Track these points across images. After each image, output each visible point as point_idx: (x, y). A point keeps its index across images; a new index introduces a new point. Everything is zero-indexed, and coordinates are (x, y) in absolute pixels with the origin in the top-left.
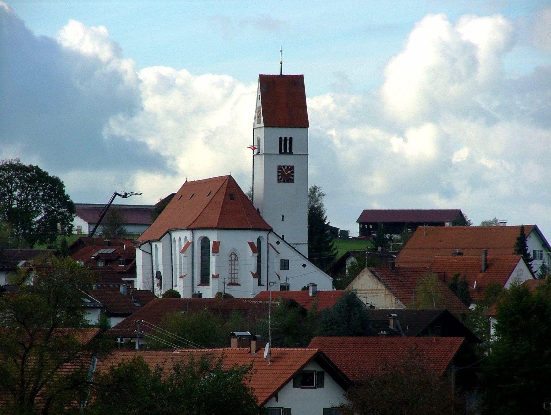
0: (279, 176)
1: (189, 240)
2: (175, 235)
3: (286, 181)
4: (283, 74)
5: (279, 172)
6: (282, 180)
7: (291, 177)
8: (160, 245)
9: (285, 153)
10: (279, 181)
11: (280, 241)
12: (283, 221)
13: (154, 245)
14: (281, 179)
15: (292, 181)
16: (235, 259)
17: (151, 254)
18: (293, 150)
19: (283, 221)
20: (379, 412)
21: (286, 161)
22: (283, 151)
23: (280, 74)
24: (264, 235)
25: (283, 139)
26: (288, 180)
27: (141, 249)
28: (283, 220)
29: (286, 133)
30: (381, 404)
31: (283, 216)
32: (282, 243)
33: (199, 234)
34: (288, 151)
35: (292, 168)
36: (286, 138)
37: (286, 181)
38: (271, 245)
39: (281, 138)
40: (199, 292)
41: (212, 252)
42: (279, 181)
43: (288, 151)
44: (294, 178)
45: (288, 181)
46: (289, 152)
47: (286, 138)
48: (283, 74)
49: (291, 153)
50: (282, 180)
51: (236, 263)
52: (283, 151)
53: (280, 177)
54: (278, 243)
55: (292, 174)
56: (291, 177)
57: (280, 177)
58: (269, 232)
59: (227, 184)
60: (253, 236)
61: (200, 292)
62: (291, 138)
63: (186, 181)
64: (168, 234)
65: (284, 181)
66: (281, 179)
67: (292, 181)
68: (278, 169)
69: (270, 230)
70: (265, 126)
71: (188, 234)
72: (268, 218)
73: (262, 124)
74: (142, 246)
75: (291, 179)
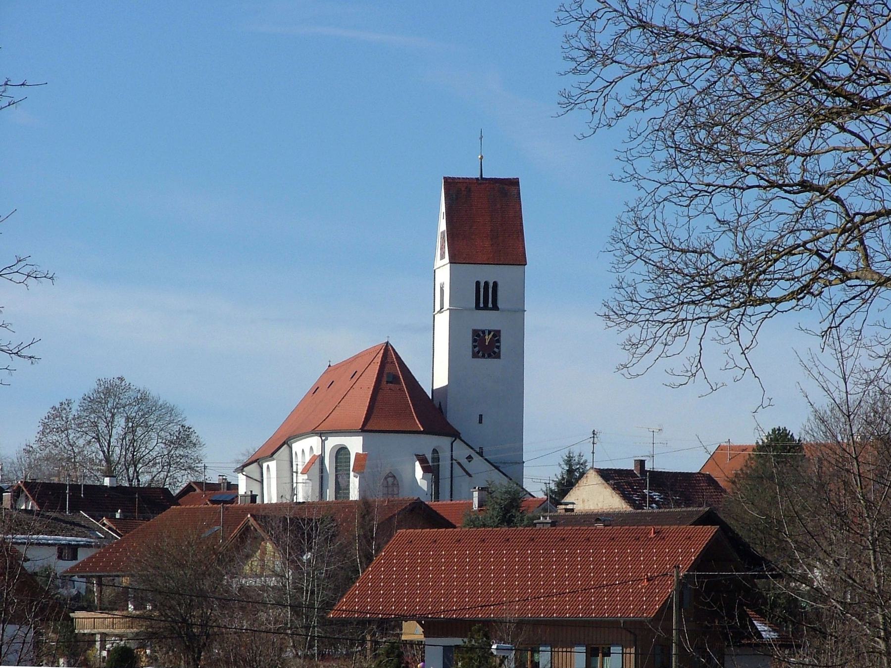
0: (475, 347)
1: (317, 452)
2: (297, 446)
3: (486, 356)
4: (483, 177)
5: (474, 341)
6: (480, 354)
7: (496, 350)
8: (273, 464)
9: (486, 308)
10: (475, 355)
11: (473, 454)
12: (481, 423)
13: (265, 465)
14: (478, 352)
15: (497, 356)
16: (393, 484)
17: (262, 482)
18: (500, 305)
19: (481, 423)
20: (738, 162)
21: (487, 320)
22: (482, 305)
23: (479, 176)
24: (443, 442)
25: (482, 285)
26: (490, 354)
27: (244, 473)
28: (480, 421)
29: (488, 273)
30: (46, 447)
31: (481, 416)
32: (477, 458)
33: (333, 442)
34: (490, 305)
35: (497, 334)
36: (486, 283)
37: (486, 356)
38: (459, 464)
39: (478, 283)
40: (251, 491)
41: (353, 471)
42: (475, 355)
43: (490, 305)
44: (500, 352)
45: (490, 356)
46: (491, 306)
47: (486, 283)
48: (483, 177)
49: (495, 307)
50: (480, 354)
51: (395, 489)
52: (482, 305)
53: (477, 349)
54: (470, 458)
55: (498, 344)
56: (496, 350)
57: (477, 349)
58: (454, 439)
59: (381, 356)
60: (427, 443)
61: (253, 493)
62: (495, 284)
63: (330, 366)
64: (286, 445)
65: (483, 356)
66: (478, 352)
67: (497, 356)
68: (473, 337)
69: (454, 434)
70: (451, 262)
71: (314, 442)
72: (452, 419)
73: (447, 259)
74: (245, 469)
75: (495, 353)
